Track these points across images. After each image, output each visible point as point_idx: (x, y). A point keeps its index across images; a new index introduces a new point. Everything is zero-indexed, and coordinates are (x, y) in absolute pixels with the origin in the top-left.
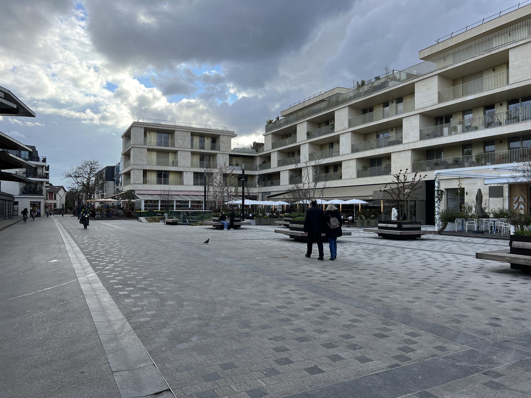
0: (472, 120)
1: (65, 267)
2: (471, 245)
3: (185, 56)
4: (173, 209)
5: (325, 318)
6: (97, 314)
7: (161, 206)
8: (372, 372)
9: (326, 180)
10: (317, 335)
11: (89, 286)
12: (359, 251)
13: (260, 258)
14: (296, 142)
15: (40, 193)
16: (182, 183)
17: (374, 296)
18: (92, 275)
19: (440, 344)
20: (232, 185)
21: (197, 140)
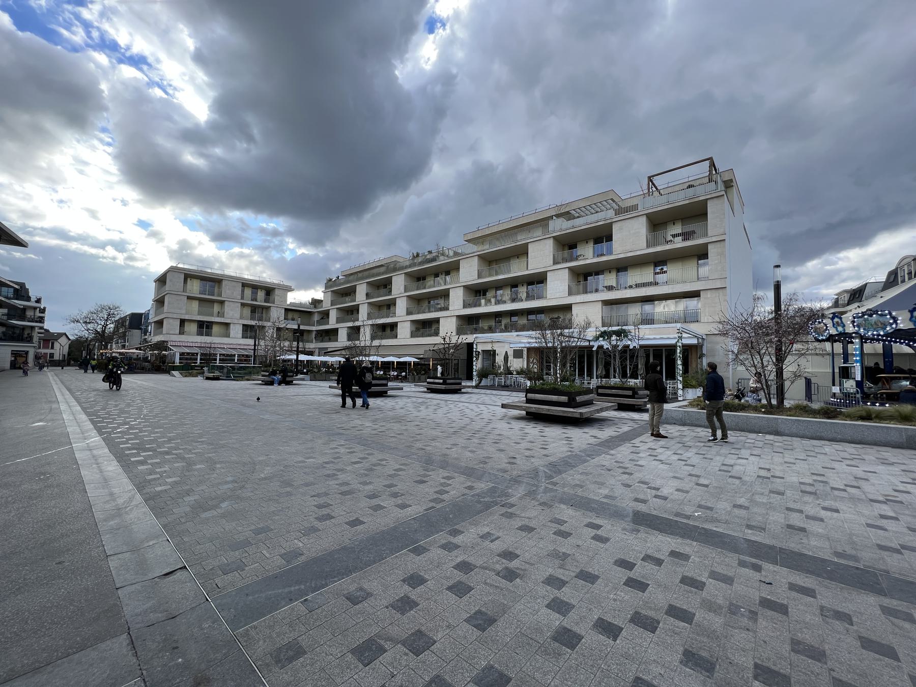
0: (502, 295)
1: (55, 431)
2: (499, 397)
3: (241, 203)
4: (197, 363)
5: (371, 470)
6: (95, 486)
7: (201, 359)
8: (410, 517)
9: (382, 339)
10: (361, 487)
11: (88, 453)
12: (409, 405)
13: (311, 414)
14: (355, 301)
15: (29, 339)
16: (228, 336)
17: (419, 445)
18: (95, 439)
19: (469, 484)
20: (287, 339)
21: (248, 292)
